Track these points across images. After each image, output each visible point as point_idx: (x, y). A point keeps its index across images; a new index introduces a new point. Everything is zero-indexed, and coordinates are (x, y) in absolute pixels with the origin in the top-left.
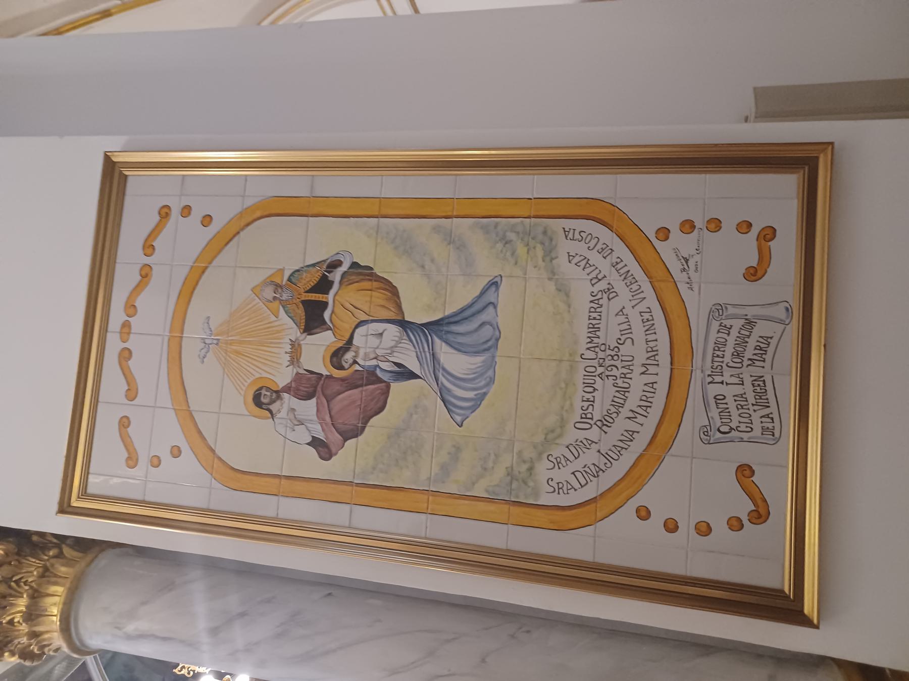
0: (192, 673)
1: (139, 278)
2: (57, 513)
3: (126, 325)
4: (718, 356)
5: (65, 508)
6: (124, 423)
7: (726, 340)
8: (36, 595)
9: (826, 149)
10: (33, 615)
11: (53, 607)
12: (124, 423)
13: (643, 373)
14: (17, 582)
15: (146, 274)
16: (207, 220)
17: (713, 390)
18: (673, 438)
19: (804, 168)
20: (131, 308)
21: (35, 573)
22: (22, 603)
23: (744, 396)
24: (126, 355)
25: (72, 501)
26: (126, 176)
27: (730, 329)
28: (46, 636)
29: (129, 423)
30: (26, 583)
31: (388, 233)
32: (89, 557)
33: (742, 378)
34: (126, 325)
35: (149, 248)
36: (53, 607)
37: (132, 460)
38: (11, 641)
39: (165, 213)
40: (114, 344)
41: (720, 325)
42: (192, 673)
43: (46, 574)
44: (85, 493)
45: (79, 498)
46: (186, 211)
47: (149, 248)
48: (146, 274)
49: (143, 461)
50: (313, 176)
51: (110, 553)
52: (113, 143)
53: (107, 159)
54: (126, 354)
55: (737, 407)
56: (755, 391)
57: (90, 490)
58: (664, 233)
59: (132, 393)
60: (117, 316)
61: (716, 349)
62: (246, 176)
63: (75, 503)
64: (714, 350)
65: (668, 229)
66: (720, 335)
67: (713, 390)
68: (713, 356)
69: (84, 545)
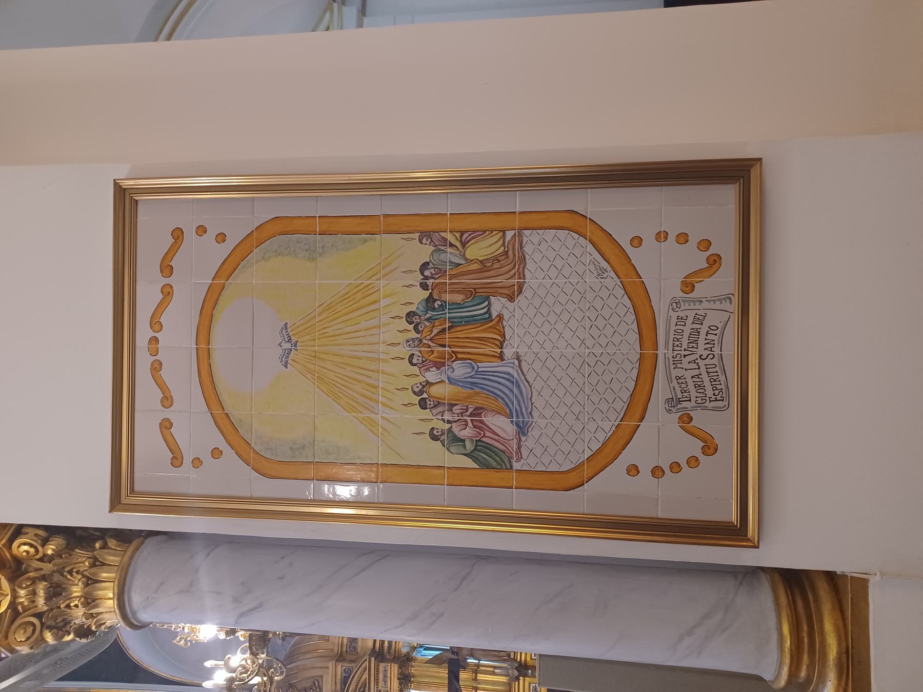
0: (189, 644)
1: (161, 296)
2: (110, 511)
3: (154, 340)
4: (678, 346)
5: (116, 504)
6: (166, 426)
7: (683, 331)
8: (91, 581)
9: (757, 163)
10: (90, 601)
11: (107, 595)
12: (166, 426)
13: (674, 368)
14: (70, 572)
15: (167, 292)
16: (221, 238)
17: (675, 373)
18: (359, 423)
19: (740, 179)
20: (156, 323)
21: (87, 564)
22: (77, 590)
23: (699, 376)
24: (156, 367)
25: (122, 500)
26: (137, 201)
27: (686, 320)
28: (101, 617)
29: (172, 424)
30: (78, 572)
31: (286, 249)
32: (132, 548)
33: (698, 363)
34: (154, 340)
35: (166, 269)
36: (107, 595)
37: (177, 460)
38: (70, 622)
39: (178, 235)
40: (144, 361)
41: (678, 319)
42: (189, 644)
43: (97, 563)
44: (133, 492)
45: (128, 496)
46: (202, 230)
47: (166, 269)
48: (167, 292)
49: (187, 460)
50: (317, 197)
51: (150, 542)
52: (121, 172)
53: (116, 185)
54: (156, 365)
55: (712, 388)
56: (697, 402)
57: (137, 488)
58: (637, 241)
59: (167, 401)
60: (144, 333)
61: (675, 340)
62: (253, 198)
63: (123, 500)
64: (674, 341)
65: (687, 234)
66: (678, 327)
67: (675, 373)
68: (673, 346)
69: (125, 537)
